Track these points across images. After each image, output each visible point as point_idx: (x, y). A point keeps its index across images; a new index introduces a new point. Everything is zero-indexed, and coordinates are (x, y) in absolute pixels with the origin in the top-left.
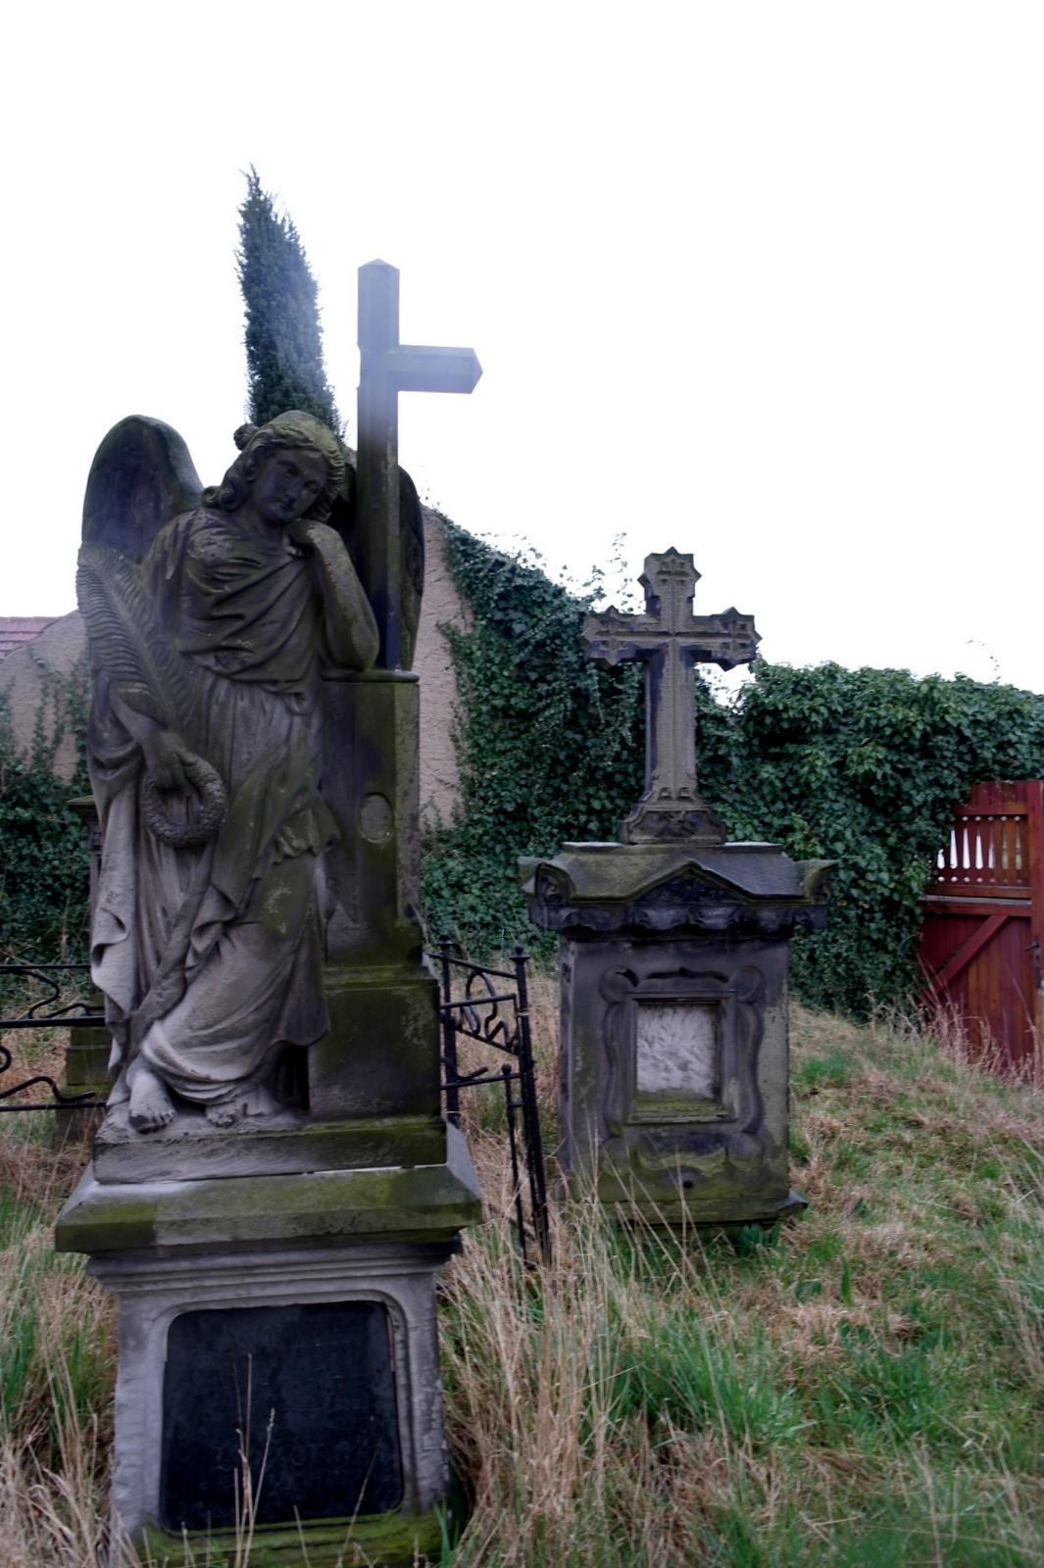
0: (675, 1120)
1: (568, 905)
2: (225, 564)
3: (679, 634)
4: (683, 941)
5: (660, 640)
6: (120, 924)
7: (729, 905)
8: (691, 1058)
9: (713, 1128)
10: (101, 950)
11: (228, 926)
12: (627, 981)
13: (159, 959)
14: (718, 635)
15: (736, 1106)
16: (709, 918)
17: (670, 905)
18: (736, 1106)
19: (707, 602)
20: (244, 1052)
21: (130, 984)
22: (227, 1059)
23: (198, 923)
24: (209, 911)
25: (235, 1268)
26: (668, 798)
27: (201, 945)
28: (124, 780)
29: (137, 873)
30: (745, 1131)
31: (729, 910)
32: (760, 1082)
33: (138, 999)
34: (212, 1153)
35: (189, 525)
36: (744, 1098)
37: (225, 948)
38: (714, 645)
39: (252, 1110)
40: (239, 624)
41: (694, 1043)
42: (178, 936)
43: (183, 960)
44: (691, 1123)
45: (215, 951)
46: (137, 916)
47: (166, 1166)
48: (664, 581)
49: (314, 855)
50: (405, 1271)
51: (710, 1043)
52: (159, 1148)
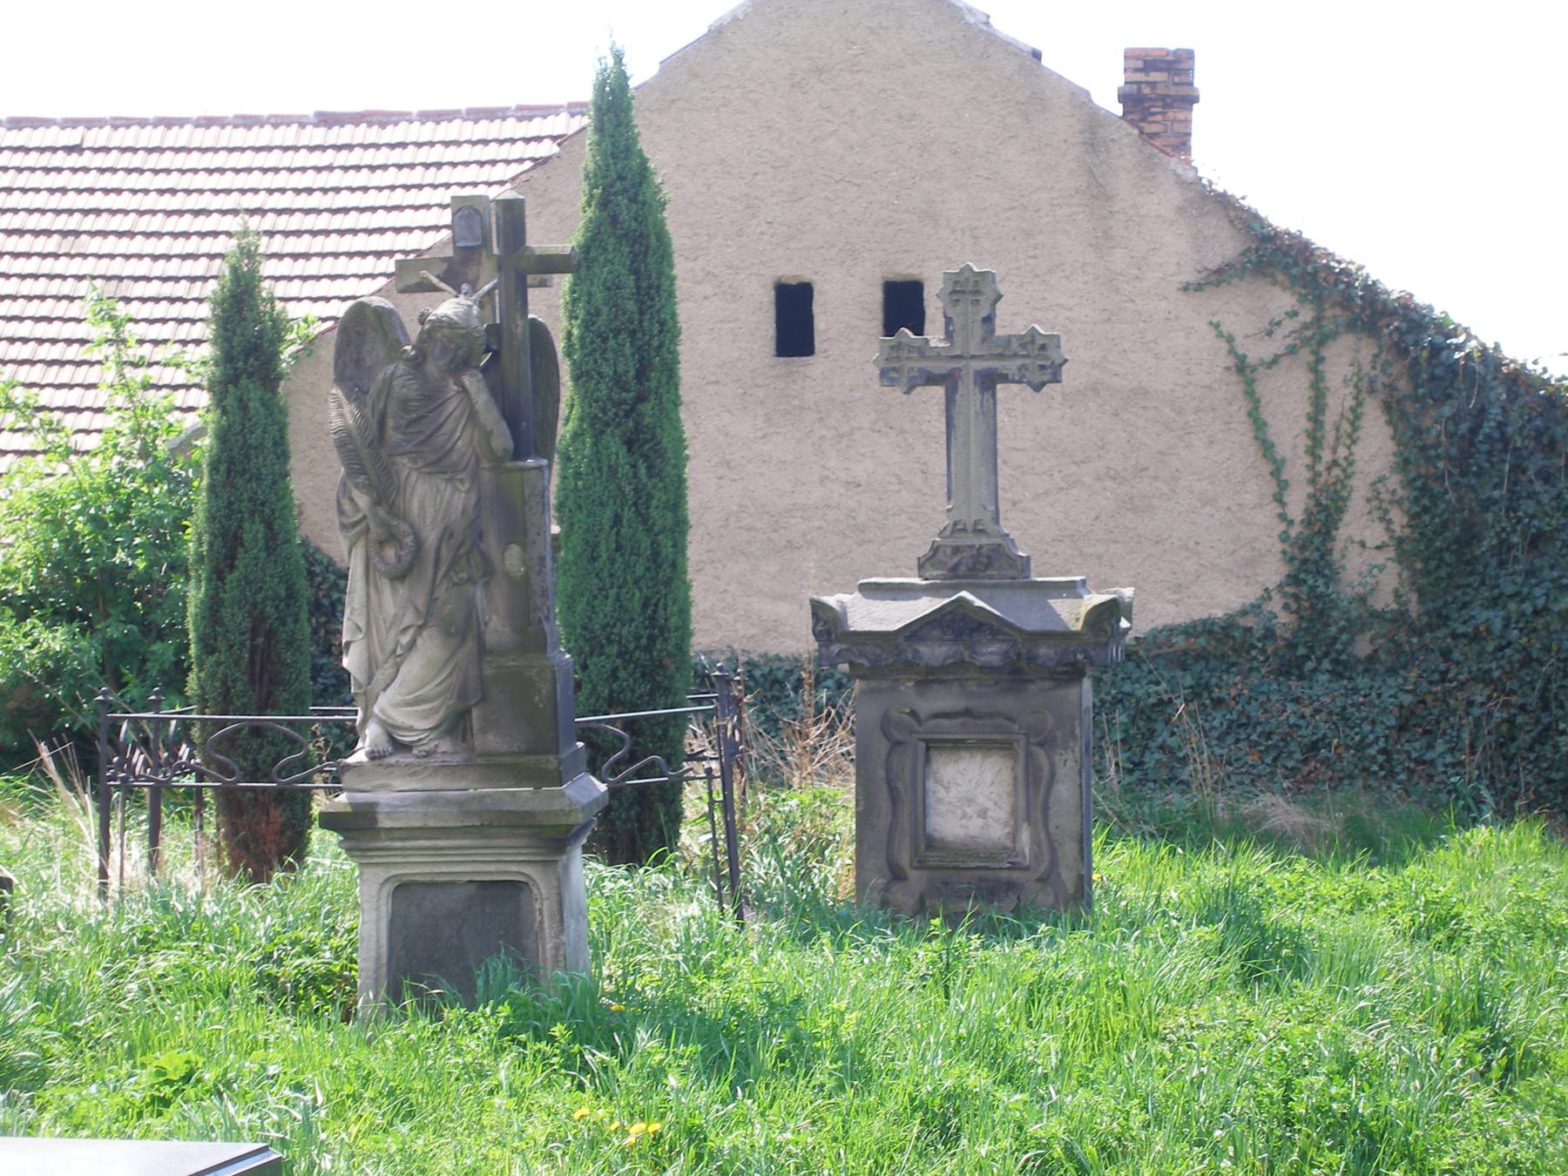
0: (962, 865)
1: (838, 640)
2: (413, 400)
3: (973, 357)
4: (967, 680)
5: (953, 365)
6: (359, 628)
7: (1004, 641)
8: (989, 805)
9: (1004, 875)
10: (348, 644)
11: (421, 628)
12: (912, 721)
13: (382, 649)
14: (1015, 355)
15: (1027, 851)
16: (984, 654)
17: (942, 640)
18: (1027, 851)
19: (1009, 322)
20: (435, 711)
21: (366, 676)
22: (425, 715)
23: (402, 627)
24: (409, 618)
25: (427, 848)
26: (964, 530)
27: (405, 639)
28: (358, 535)
29: (368, 595)
30: (1038, 880)
31: (1004, 647)
32: (1052, 829)
33: (370, 678)
34: (414, 774)
35: (393, 373)
36: (1036, 842)
37: (419, 642)
38: (1010, 367)
39: (441, 750)
40: (422, 437)
41: (992, 789)
42: (393, 633)
43: (395, 650)
44: (979, 868)
45: (412, 645)
46: (368, 623)
47: (386, 781)
48: (958, 301)
49: (474, 583)
50: (538, 858)
51: (1009, 789)
52: (381, 769)
